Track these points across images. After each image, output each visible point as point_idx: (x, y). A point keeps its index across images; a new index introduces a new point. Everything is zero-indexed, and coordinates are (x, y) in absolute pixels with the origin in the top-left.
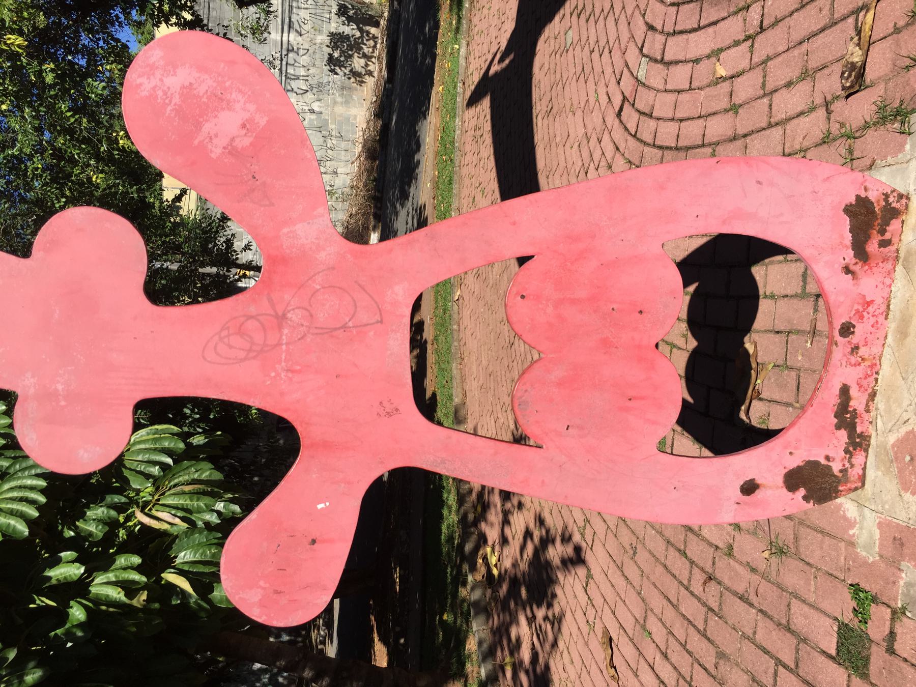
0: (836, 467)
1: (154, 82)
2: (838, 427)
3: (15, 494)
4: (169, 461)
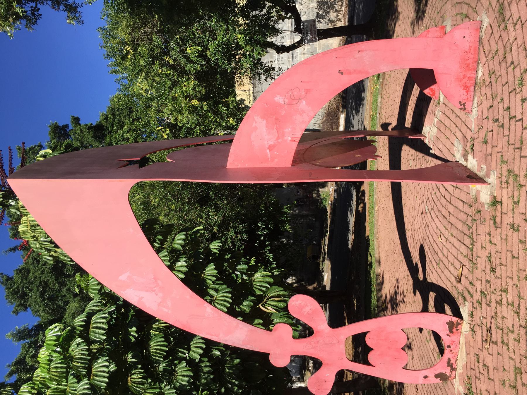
0: (448, 374)
1: (294, 303)
2: (448, 366)
3: (222, 298)
4: (269, 286)
